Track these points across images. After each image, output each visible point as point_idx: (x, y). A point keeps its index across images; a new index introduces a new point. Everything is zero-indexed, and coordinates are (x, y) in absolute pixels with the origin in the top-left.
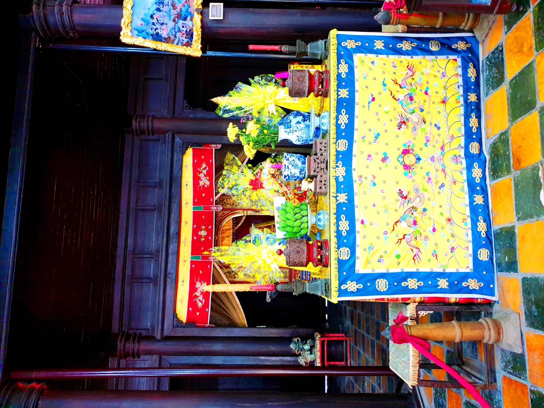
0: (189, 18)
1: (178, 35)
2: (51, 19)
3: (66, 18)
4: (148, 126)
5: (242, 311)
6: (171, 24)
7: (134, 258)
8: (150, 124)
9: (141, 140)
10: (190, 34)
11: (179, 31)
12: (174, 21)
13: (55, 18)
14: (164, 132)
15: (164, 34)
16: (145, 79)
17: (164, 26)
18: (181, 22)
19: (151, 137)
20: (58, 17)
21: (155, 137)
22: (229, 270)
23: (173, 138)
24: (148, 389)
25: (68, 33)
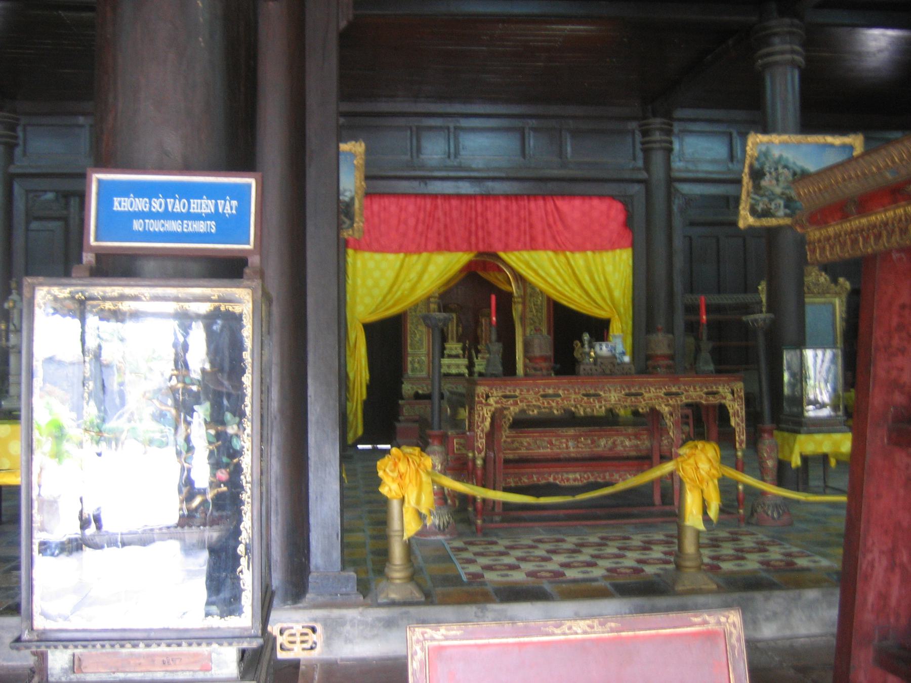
0: (788, 211)
1: (766, 200)
2: (776, 40)
3: (778, 58)
4: (655, 142)
5: (785, 362)
6: (778, 190)
7: (411, 128)
8: (657, 145)
9: (633, 133)
10: (766, 213)
11: (771, 200)
12: (783, 194)
13: (778, 45)
14: (647, 167)
15: (765, 182)
16: (731, 135)
17: (774, 182)
18: (782, 203)
19: (638, 146)
20: (778, 48)
21: (640, 154)
22: (737, 546)
23: (639, 181)
24: (840, 551)
25: (762, 57)
